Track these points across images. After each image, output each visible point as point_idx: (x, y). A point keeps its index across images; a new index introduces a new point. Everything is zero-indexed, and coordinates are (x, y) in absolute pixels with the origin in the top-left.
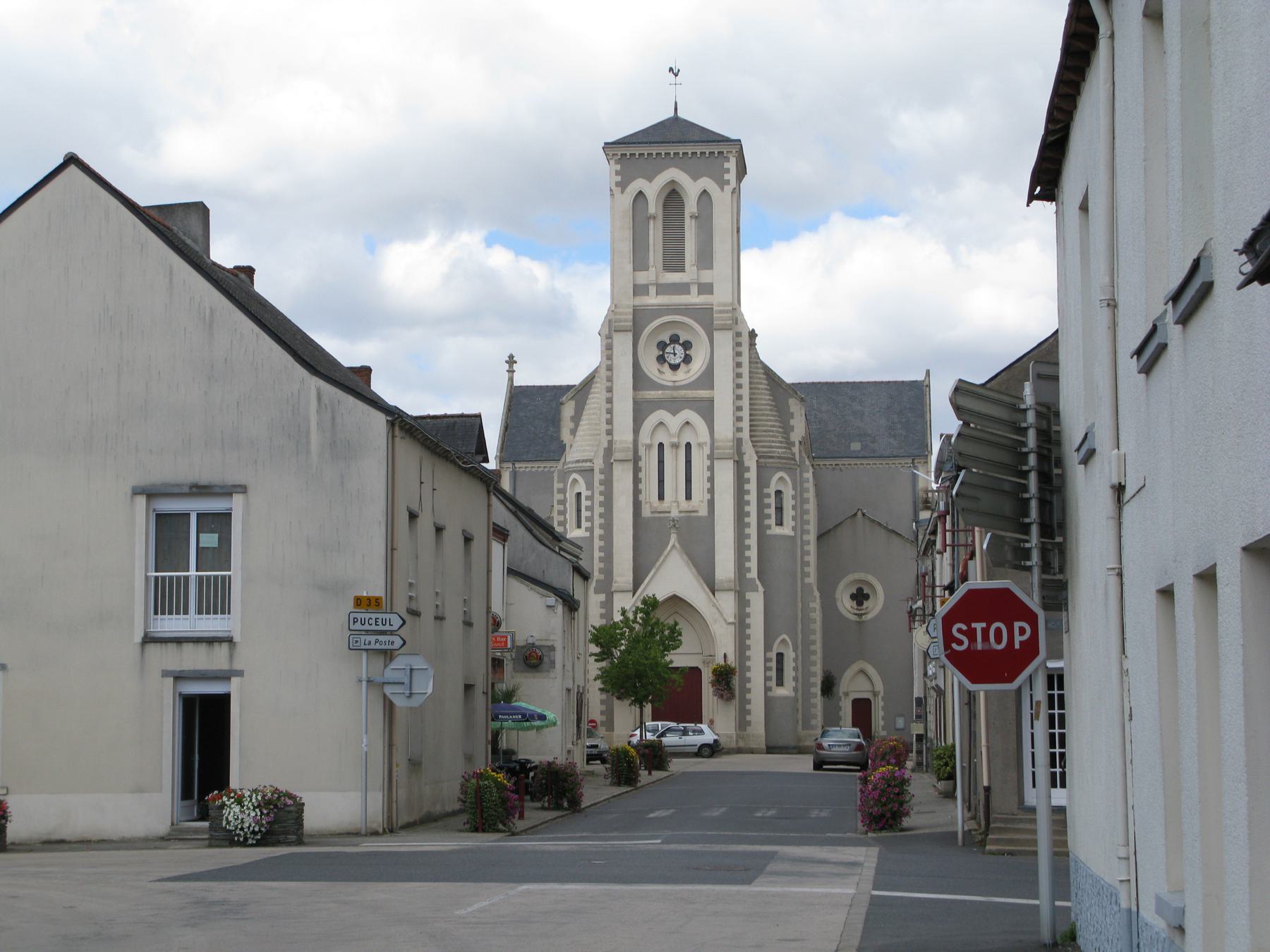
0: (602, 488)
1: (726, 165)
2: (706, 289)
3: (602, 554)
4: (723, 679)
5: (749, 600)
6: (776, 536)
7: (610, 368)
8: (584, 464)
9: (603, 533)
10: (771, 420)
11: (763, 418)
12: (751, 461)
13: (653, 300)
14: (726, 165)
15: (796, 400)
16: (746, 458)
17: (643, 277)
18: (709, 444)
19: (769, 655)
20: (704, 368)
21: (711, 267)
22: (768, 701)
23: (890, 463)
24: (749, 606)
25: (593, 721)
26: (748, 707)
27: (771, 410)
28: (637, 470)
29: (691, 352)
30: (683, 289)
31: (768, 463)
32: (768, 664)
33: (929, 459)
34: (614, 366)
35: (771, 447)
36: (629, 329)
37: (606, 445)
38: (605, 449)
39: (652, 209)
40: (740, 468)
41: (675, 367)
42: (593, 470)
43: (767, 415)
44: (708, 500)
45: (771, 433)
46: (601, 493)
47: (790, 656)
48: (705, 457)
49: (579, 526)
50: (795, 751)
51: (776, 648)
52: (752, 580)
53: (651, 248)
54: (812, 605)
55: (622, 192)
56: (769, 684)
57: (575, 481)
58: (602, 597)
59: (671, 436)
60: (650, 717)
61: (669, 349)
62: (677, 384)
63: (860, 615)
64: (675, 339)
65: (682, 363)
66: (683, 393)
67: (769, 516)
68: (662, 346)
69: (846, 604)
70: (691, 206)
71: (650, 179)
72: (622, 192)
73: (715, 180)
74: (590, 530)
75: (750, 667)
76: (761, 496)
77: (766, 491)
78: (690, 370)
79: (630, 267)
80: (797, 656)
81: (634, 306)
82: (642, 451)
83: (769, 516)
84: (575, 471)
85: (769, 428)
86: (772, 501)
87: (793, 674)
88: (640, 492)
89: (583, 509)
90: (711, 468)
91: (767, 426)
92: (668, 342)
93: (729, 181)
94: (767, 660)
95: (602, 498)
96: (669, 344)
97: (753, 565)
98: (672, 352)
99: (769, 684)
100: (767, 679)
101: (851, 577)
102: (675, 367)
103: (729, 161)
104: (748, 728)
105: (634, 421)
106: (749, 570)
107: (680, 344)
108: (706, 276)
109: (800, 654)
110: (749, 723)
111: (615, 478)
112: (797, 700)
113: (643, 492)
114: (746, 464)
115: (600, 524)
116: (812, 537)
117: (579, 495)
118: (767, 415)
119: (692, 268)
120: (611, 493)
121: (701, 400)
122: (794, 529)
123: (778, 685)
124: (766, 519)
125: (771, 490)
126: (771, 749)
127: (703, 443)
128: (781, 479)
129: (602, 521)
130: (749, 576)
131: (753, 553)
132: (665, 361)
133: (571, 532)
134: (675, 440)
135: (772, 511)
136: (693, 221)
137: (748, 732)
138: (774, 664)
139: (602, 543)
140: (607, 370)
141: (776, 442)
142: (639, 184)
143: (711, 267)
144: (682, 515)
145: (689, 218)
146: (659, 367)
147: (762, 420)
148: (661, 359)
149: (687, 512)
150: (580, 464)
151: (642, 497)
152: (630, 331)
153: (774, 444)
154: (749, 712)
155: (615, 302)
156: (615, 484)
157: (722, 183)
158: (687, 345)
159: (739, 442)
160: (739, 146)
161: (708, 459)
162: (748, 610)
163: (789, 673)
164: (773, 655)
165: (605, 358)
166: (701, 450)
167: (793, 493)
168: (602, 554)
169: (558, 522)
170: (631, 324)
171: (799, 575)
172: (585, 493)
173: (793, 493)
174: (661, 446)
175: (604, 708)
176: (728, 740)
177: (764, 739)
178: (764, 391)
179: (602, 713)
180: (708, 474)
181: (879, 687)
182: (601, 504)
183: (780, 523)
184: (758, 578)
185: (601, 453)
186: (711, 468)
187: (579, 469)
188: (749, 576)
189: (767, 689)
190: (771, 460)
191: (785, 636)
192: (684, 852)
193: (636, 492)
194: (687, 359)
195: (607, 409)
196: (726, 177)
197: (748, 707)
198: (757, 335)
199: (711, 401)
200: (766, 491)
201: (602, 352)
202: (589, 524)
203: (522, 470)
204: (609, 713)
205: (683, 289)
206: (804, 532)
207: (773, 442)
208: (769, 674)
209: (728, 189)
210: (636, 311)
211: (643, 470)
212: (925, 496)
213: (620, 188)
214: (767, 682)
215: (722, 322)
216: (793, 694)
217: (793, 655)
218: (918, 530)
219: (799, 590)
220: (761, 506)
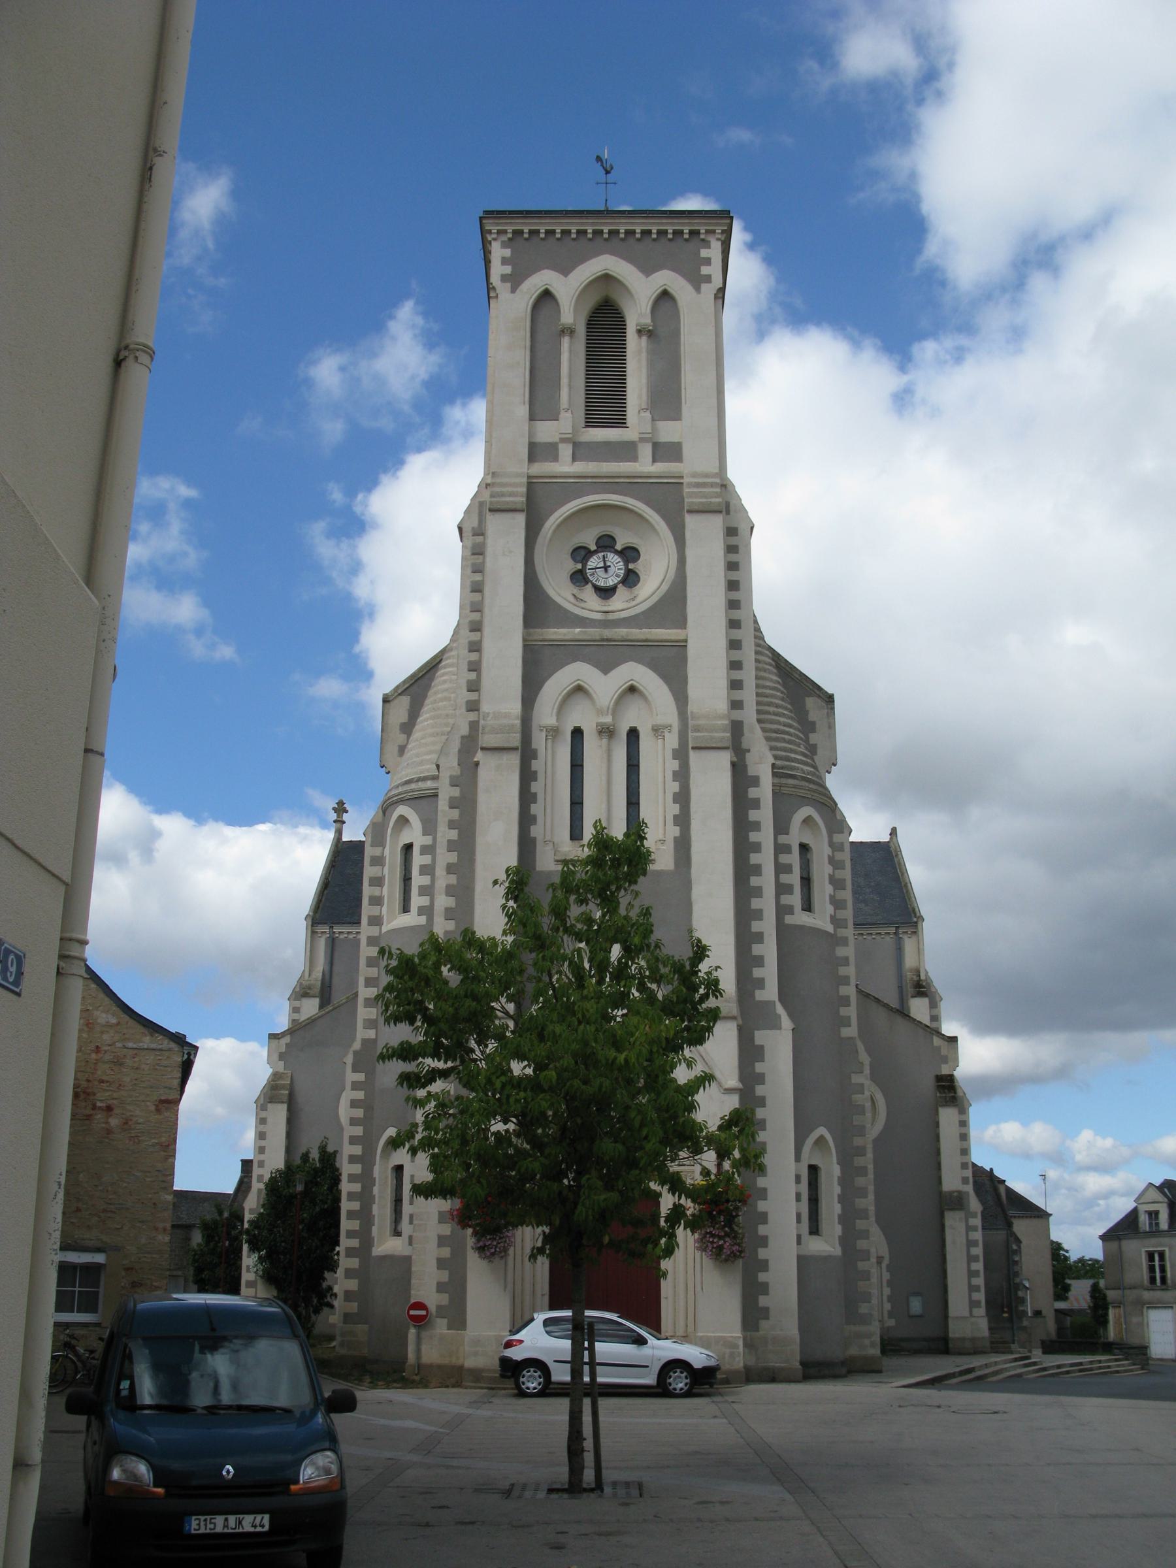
0: (455, 814)
1: (704, 253)
2: (668, 451)
4: (720, 1213)
5: (762, 1047)
6: (801, 928)
7: (475, 647)
8: (421, 785)
9: (453, 905)
10: (784, 715)
11: (772, 709)
12: (761, 764)
13: (565, 466)
15: (819, 701)
16: (750, 759)
17: (547, 431)
18: (676, 729)
20: (665, 587)
21: (677, 416)
23: (865, 933)
24: (763, 1061)
25: (419, 1306)
26: (762, 1277)
27: (783, 699)
28: (527, 776)
30: (627, 451)
31: (786, 785)
33: (919, 927)
34: (484, 665)
35: (788, 759)
36: (519, 506)
37: (465, 730)
38: (463, 737)
39: (568, 316)
40: (741, 779)
41: (606, 593)
42: (436, 795)
43: (777, 706)
44: (675, 838)
45: (786, 737)
46: (452, 825)
47: (832, 1171)
48: (669, 754)
49: (406, 909)
50: (844, 1370)
51: (807, 1158)
52: (769, 1004)
53: (564, 381)
54: (856, 1079)
57: (403, 821)
59: (600, 712)
60: (546, 1298)
61: (595, 561)
62: (611, 617)
64: (606, 543)
65: (620, 586)
66: (622, 632)
68: (581, 554)
70: (637, 313)
71: (565, 271)
72: (513, 290)
73: (684, 275)
74: (424, 911)
75: (765, 1190)
79: (523, 411)
81: (529, 477)
82: (539, 741)
84: (402, 801)
85: (782, 728)
88: (533, 820)
89: (415, 872)
90: (682, 775)
91: (779, 723)
92: (593, 548)
93: (710, 276)
96: (596, 552)
97: (769, 972)
98: (602, 565)
102: (606, 593)
103: (709, 247)
104: (764, 1324)
105: (524, 682)
106: (760, 983)
107: (617, 552)
108: (668, 431)
110: (765, 1313)
113: (540, 820)
114: (751, 771)
117: (408, 848)
118: (777, 706)
119: (643, 414)
120: (473, 822)
121: (660, 645)
122: (834, 920)
123: (811, 1233)
127: (665, 727)
128: (808, 821)
129: (453, 879)
130: (760, 996)
131: (768, 950)
132: (586, 581)
133: (389, 923)
134: (608, 719)
136: (644, 339)
137: (761, 1333)
140: (472, 591)
141: (795, 752)
143: (677, 416)
145: (636, 336)
146: (576, 591)
147: (768, 713)
148: (579, 578)
150: (413, 786)
151: (535, 831)
152: (522, 511)
153: (793, 755)
154: (764, 1288)
155: (492, 470)
157: (697, 281)
158: (630, 554)
159: (737, 728)
160: (728, 221)
161: (674, 758)
162: (759, 1067)
163: (831, 1208)
165: (469, 570)
166: (660, 741)
169: (369, 917)
170: (524, 499)
174: (577, 733)
175: (444, 1276)
176: (728, 1351)
177: (796, 1348)
178: (768, 667)
179: (441, 1288)
180: (675, 787)
183: (808, 907)
184: (780, 1000)
185: (455, 746)
186: (682, 775)
187: (409, 796)
188: (760, 996)
190: (791, 781)
191: (822, 1131)
193: (526, 820)
194: (630, 579)
195: (470, 663)
197: (762, 1277)
199: (682, 645)
201: (464, 559)
202: (425, 901)
203: (342, 937)
204: (455, 1288)
205: (627, 451)
207: (791, 751)
209: (709, 290)
210: (531, 485)
211: (541, 776)
212: (915, 978)
213: (508, 285)
215: (704, 500)
216: (837, 1251)
217: (837, 1170)
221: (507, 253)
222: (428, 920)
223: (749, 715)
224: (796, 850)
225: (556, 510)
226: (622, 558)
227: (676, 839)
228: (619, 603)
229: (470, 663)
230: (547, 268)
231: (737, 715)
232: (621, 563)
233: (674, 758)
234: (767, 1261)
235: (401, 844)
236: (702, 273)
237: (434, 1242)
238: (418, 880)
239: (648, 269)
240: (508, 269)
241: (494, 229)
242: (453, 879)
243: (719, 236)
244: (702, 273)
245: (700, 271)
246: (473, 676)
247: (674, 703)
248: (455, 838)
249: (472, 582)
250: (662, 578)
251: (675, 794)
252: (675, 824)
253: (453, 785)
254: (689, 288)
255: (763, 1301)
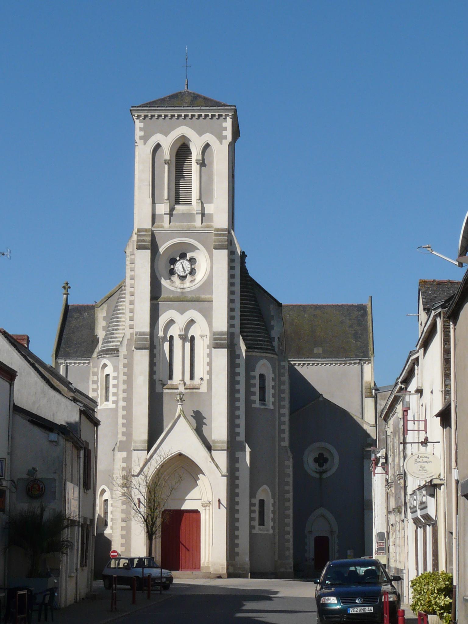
1: (224, 125)
3: (125, 421)
14: (224, 125)
19: (253, 501)
20: (205, 278)
22: (252, 537)
29: (196, 267)
32: (253, 508)
46: (124, 374)
49: (107, 399)
52: (241, 443)
54: (286, 463)
55: (145, 144)
56: (253, 523)
58: (124, 454)
63: (321, 473)
67: (254, 394)
69: (310, 465)
71: (166, 134)
76: (248, 378)
77: (252, 374)
78: (194, 280)
80: (275, 502)
83: (254, 394)
86: (257, 381)
87: (271, 515)
93: (226, 128)
94: (251, 505)
95: (125, 378)
97: (242, 430)
99: (253, 523)
100: (252, 519)
101: (318, 444)
102: (183, 278)
106: (238, 434)
107: (187, 260)
109: (277, 501)
110: (237, 554)
111: (135, 362)
112: (275, 536)
115: (123, 398)
116: (286, 411)
117: (108, 375)
123: (260, 525)
124: (252, 395)
125: (257, 374)
126: (254, 575)
127: (204, 336)
129: (125, 395)
130: (238, 439)
131: (242, 422)
133: (101, 405)
135: (257, 389)
138: (257, 508)
139: (125, 413)
142: (157, 138)
144: (188, 391)
149: (190, 389)
156: (135, 367)
157: (221, 138)
158: (192, 261)
162: (237, 465)
163: (269, 515)
164: (256, 501)
167: (273, 376)
168: (125, 421)
171: (277, 439)
172: (112, 375)
173: (273, 376)
179: (122, 545)
180: (208, 368)
181: (336, 529)
182: (124, 382)
188: (238, 439)
189: (252, 527)
192: (365, 358)
194: (193, 272)
196: (224, 133)
198: (246, 256)
200: (252, 374)
202: (115, 398)
206: (281, 407)
208: (253, 515)
213: (142, 141)
214: (252, 522)
217: (272, 501)
218: (376, 396)
219: (277, 451)
220: (248, 385)
221: (142, 125)
222: (116, 406)
223: (237, 329)
224: (258, 377)
225: (163, 245)
226: (190, 263)
227: (208, 380)
228: (187, 283)
229: (130, 325)
230: (158, 133)
231: (232, 330)
232: (189, 265)
233: (208, 348)
234: (238, 536)
235: (105, 374)
236: (223, 135)
237: (120, 520)
238: (112, 390)
239: (200, 133)
240: (142, 134)
241: (136, 115)
242: (125, 395)
243: (231, 117)
244: (223, 135)
245: (222, 134)
246: (131, 314)
247: (208, 326)
248: (126, 379)
249: (130, 275)
250: (204, 274)
251: (208, 363)
252: (208, 374)
253: (124, 401)
254: (218, 142)
255: (237, 550)
